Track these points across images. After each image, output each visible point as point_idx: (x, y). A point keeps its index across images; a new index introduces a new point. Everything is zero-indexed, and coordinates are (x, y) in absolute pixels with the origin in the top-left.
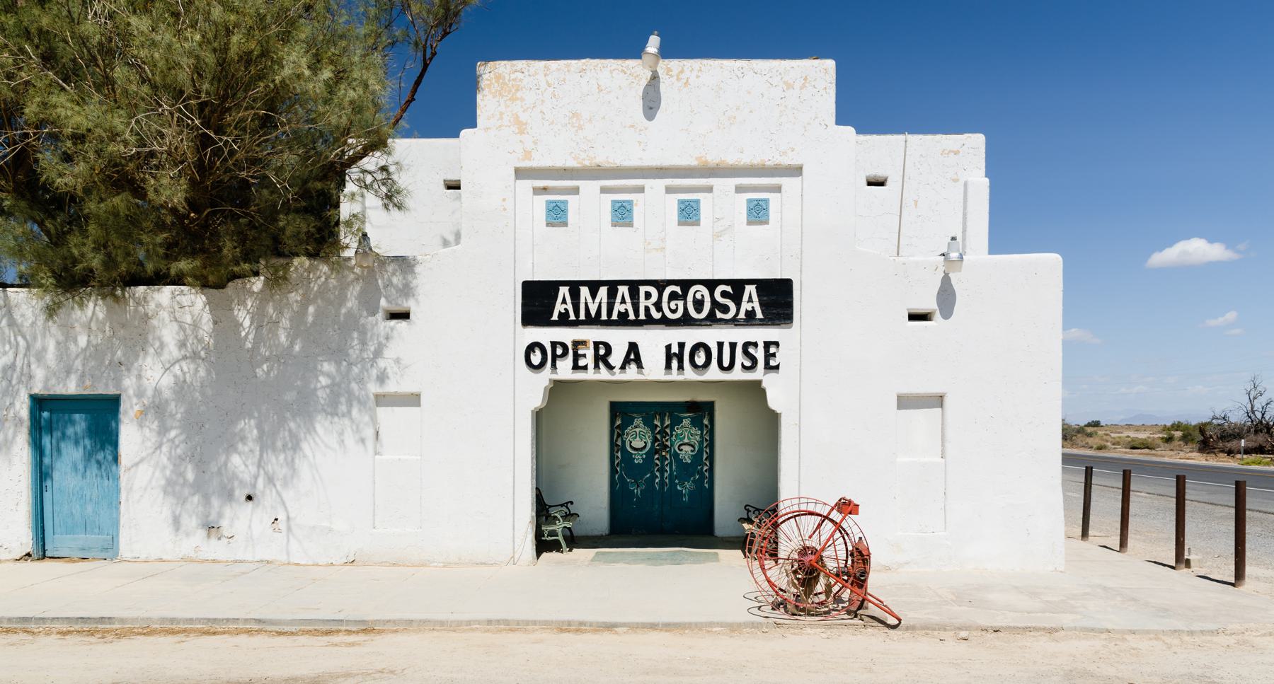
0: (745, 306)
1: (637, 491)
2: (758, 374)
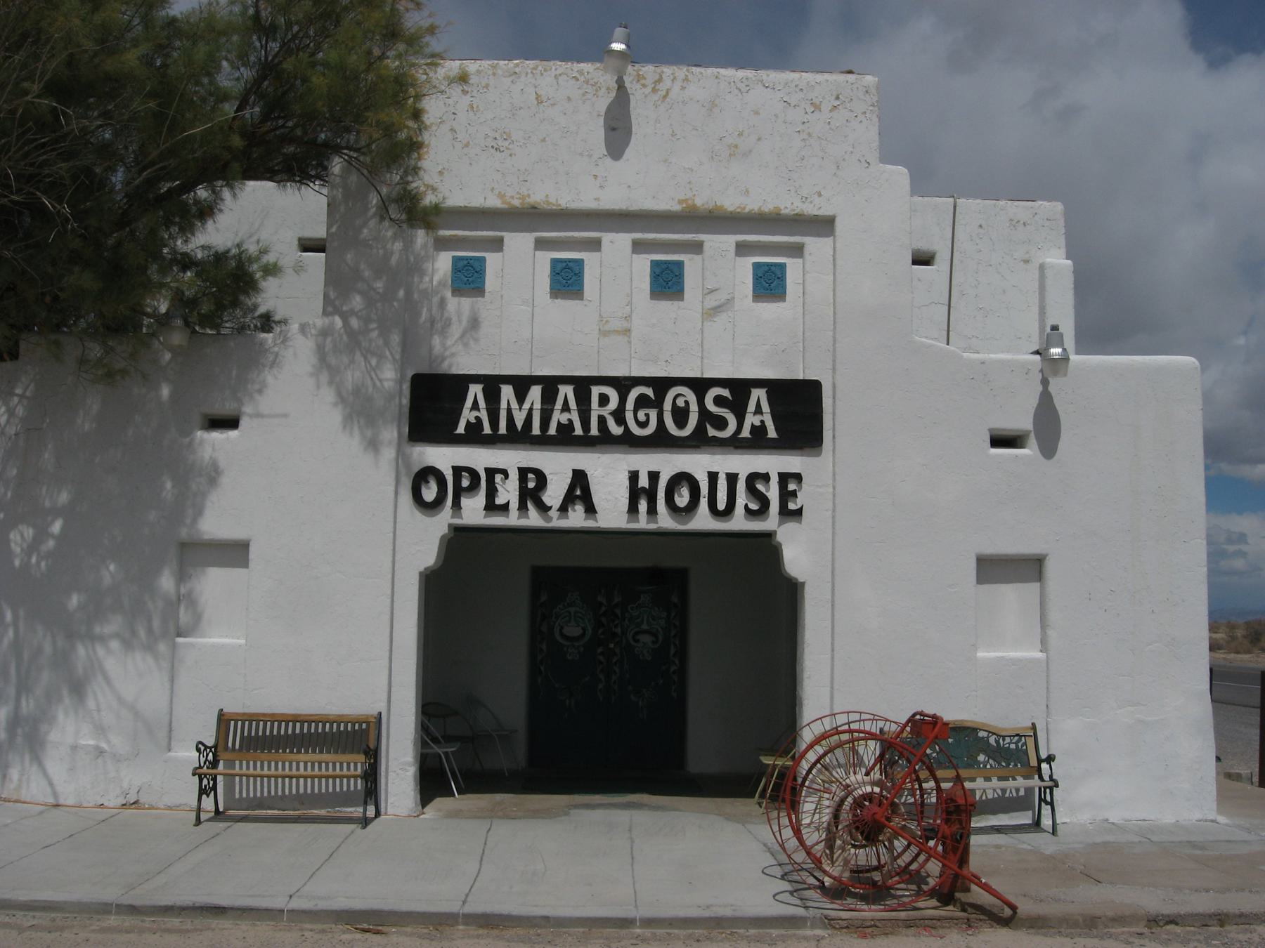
0: (751, 420)
2: (771, 522)
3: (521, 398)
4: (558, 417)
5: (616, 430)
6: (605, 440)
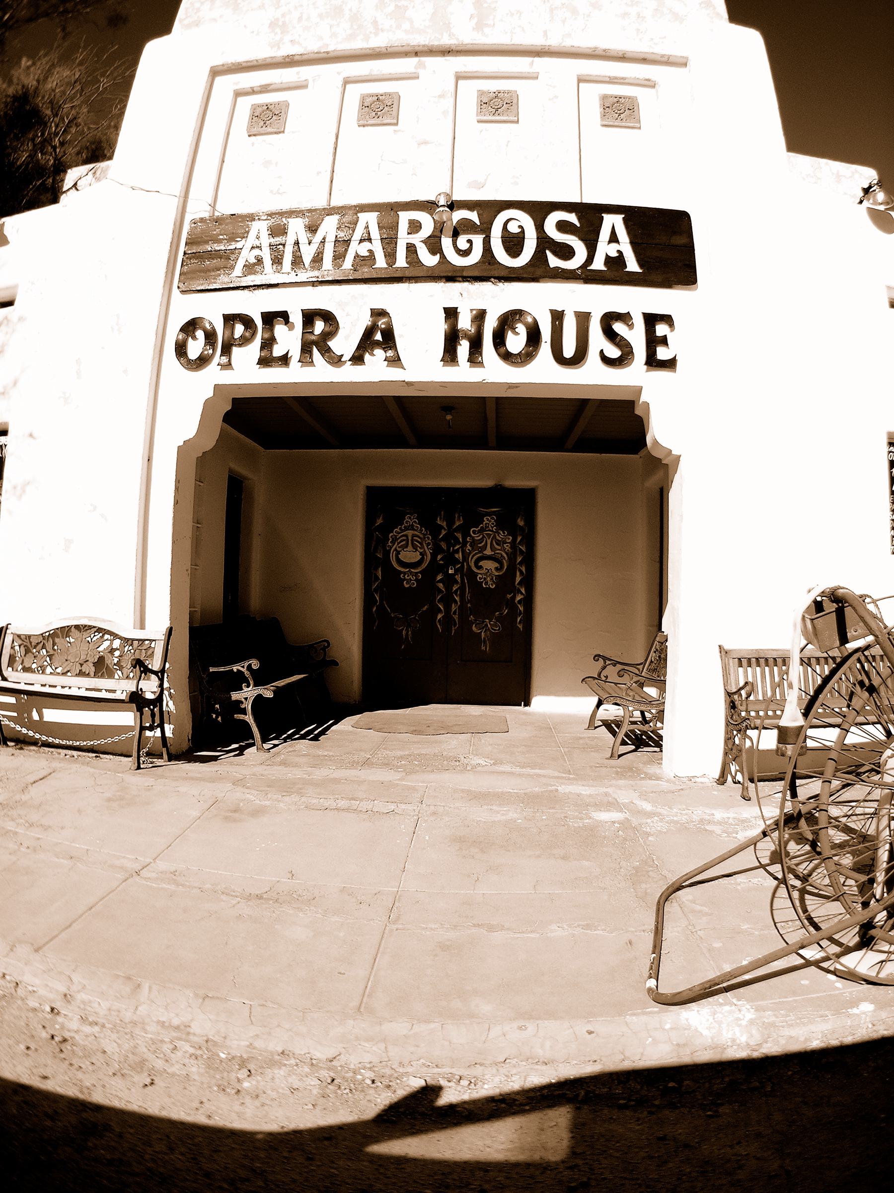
0: (604, 249)
2: (635, 374)
3: (312, 229)
4: (357, 248)
5: (429, 260)
6: (416, 274)
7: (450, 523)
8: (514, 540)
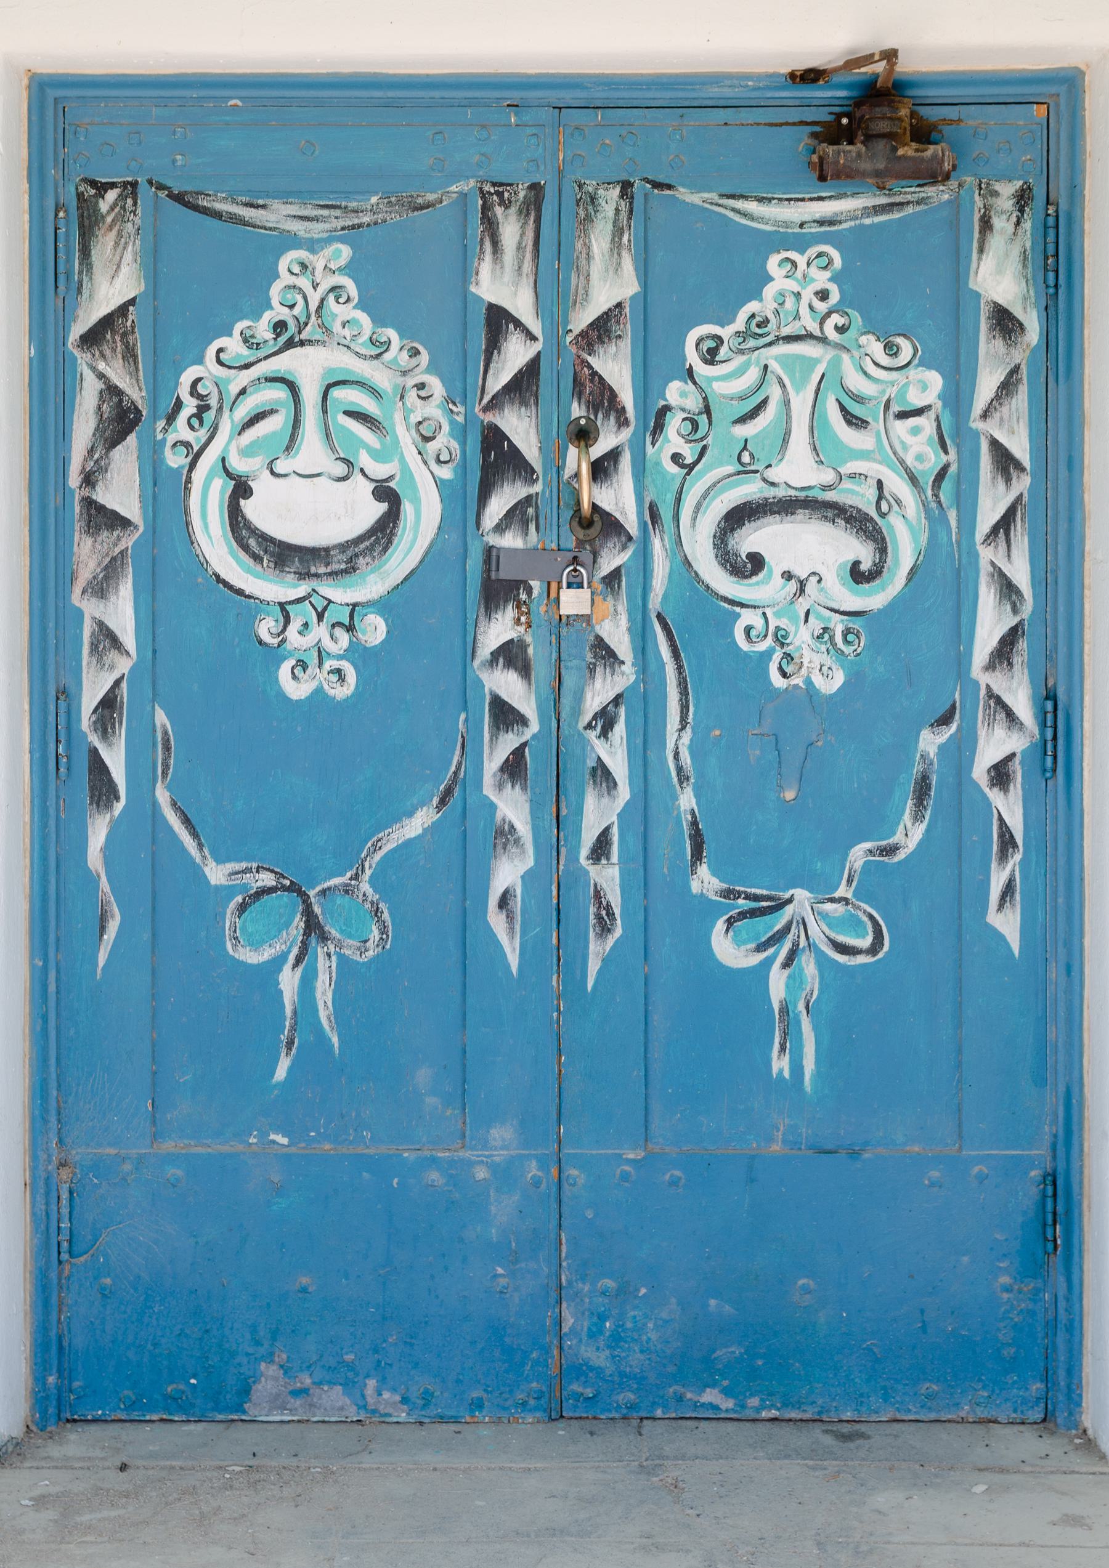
1: (311, 989)
7: (556, 283)
8: (957, 396)
